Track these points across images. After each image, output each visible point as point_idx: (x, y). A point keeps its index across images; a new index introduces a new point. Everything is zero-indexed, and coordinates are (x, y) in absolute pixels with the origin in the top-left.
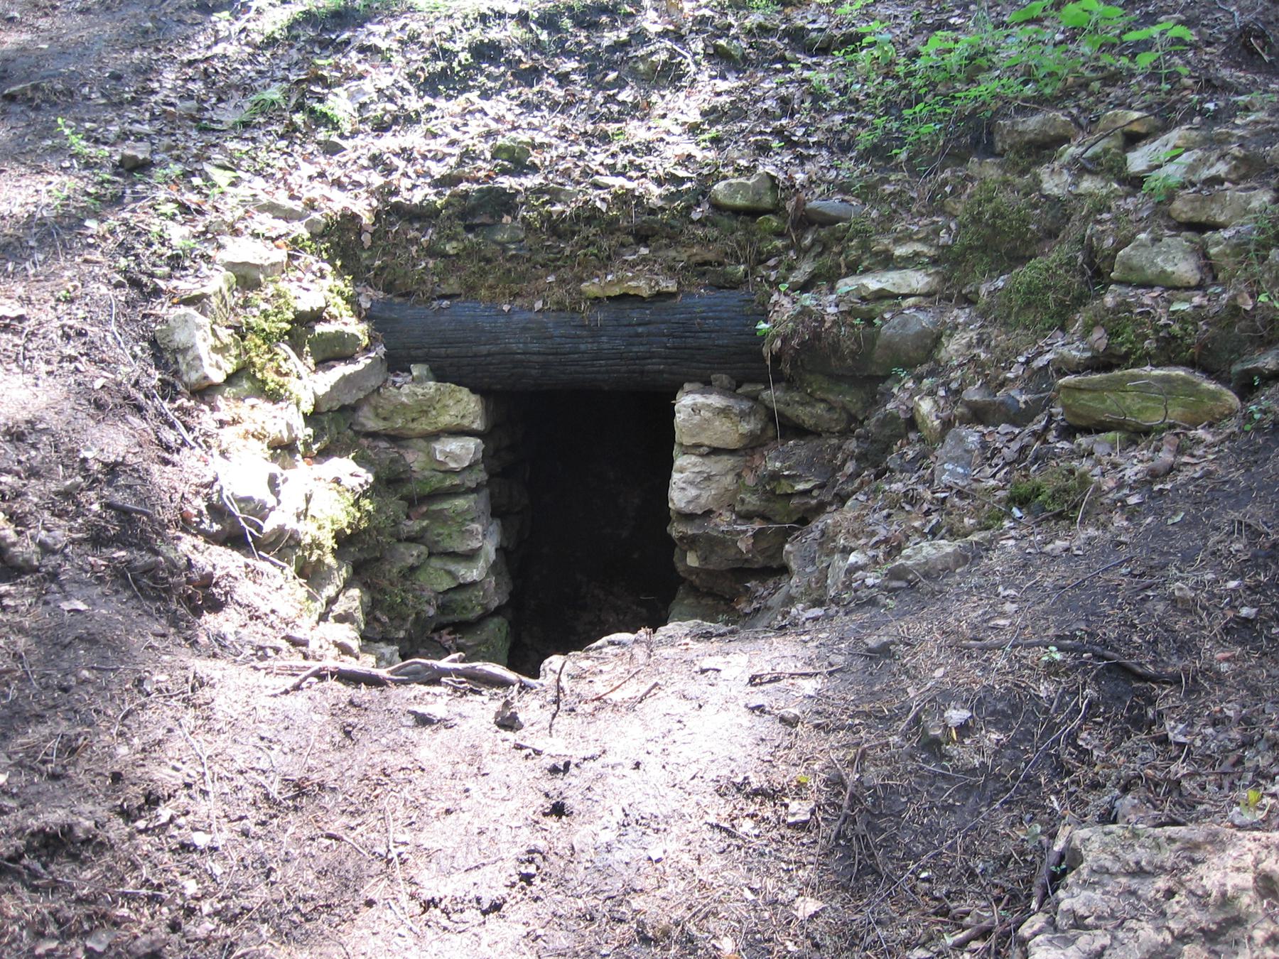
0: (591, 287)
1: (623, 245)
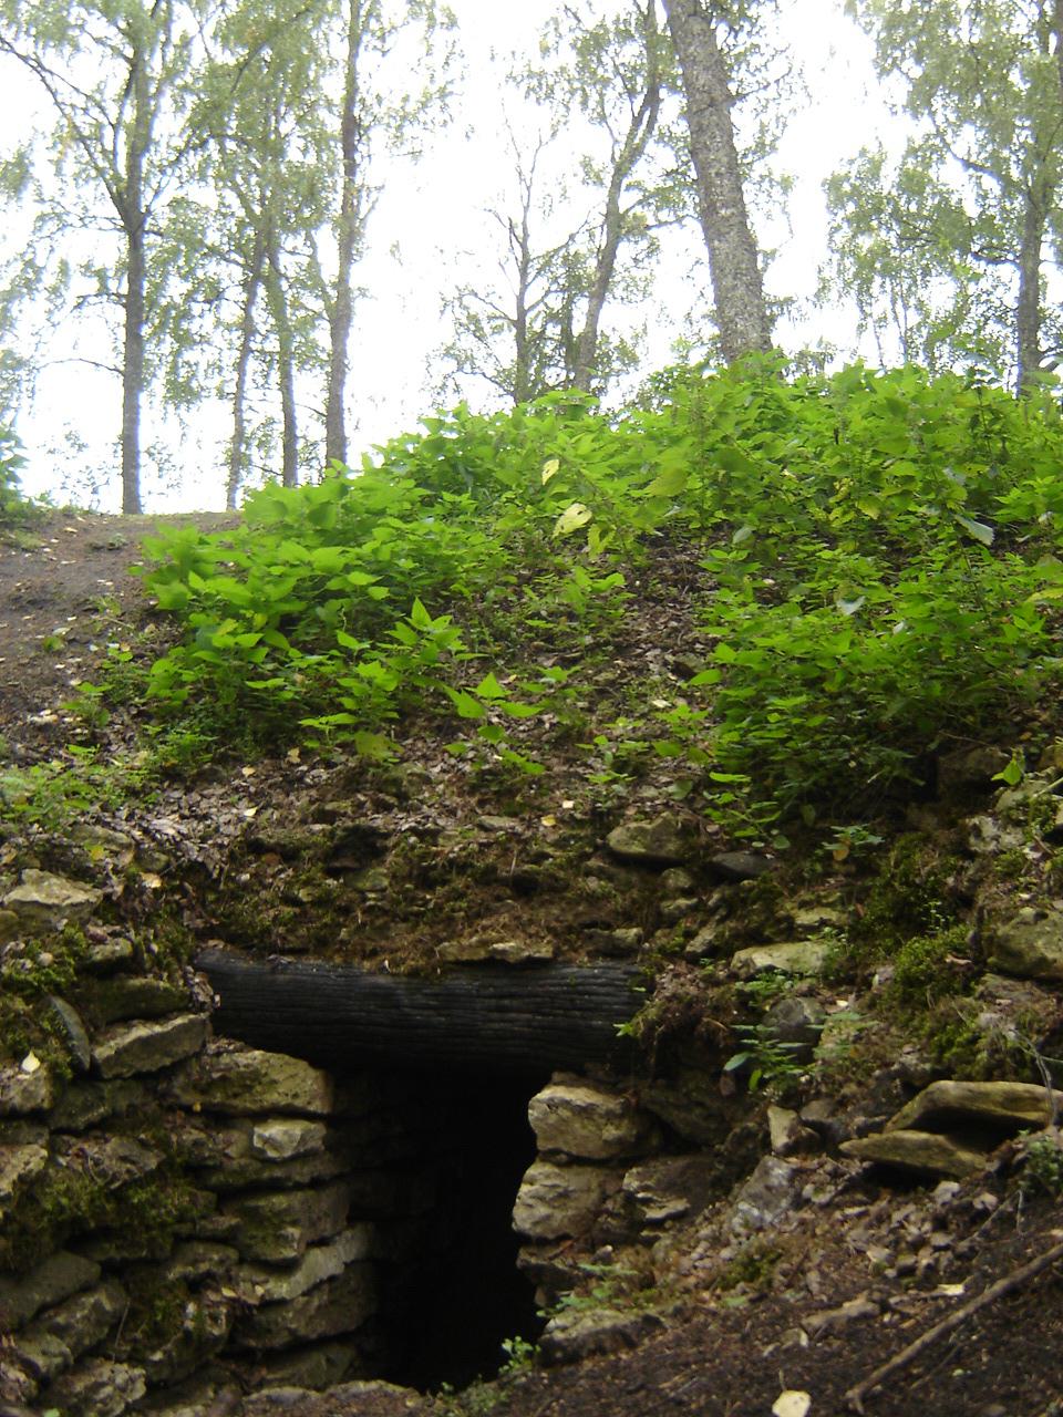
0: (450, 949)
1: (499, 899)
